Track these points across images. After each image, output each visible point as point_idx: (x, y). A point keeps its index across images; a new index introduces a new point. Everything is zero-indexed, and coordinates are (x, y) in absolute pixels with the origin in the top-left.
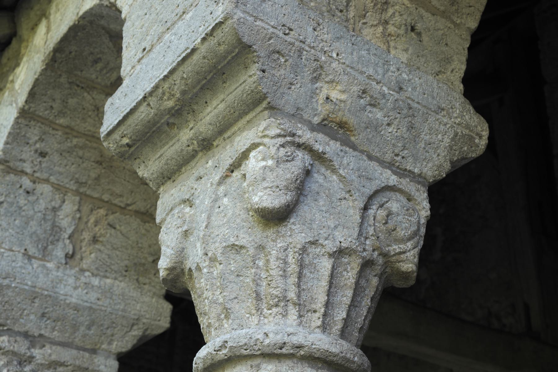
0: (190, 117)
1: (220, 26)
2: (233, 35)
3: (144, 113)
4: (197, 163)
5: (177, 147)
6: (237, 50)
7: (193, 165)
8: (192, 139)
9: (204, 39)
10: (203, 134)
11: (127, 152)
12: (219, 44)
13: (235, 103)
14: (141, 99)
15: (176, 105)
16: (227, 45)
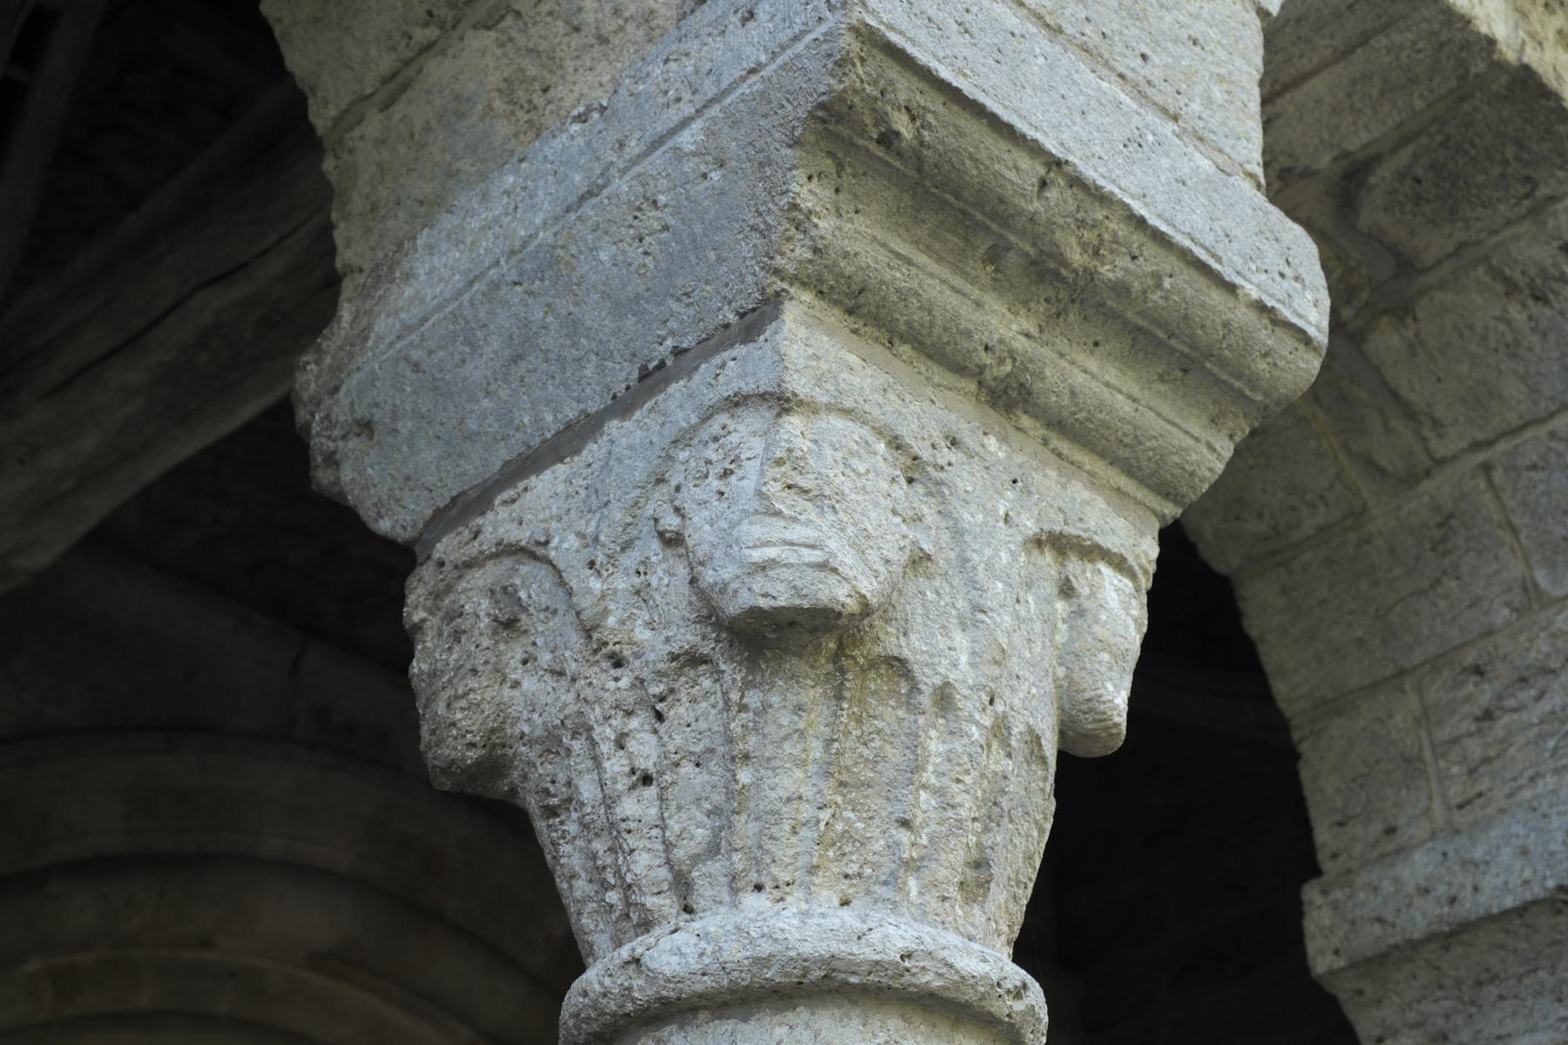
0: (1042, 310)
1: (1299, 340)
2: (1296, 384)
3: (1020, 173)
4: (950, 389)
5: (965, 310)
6: (1259, 398)
7: (936, 379)
8: (1012, 354)
9: (1260, 307)
10: (1041, 385)
11: (863, 132)
12: (1265, 355)
13: (1150, 440)
14: (1050, 154)
15: (1075, 271)
16: (1272, 377)
